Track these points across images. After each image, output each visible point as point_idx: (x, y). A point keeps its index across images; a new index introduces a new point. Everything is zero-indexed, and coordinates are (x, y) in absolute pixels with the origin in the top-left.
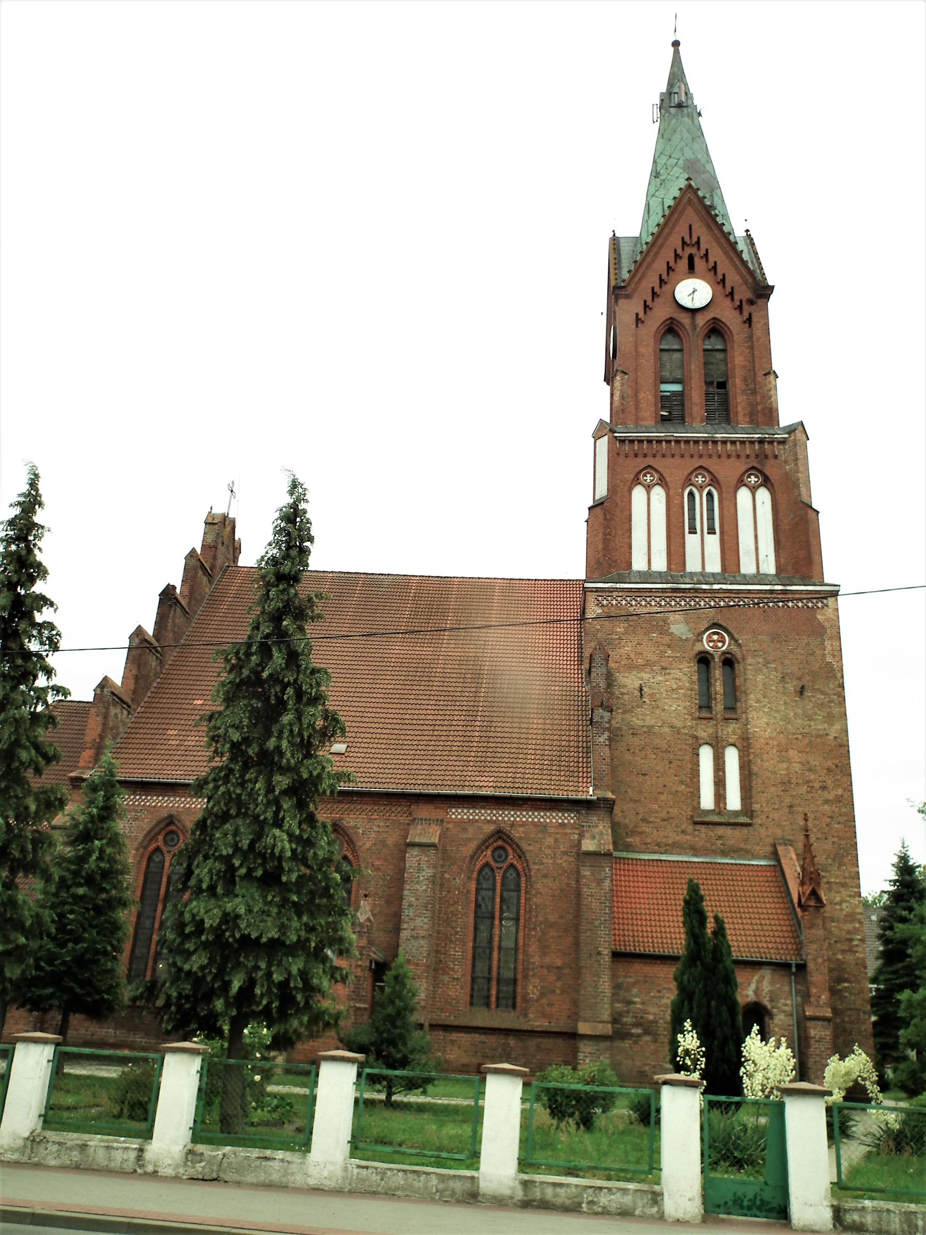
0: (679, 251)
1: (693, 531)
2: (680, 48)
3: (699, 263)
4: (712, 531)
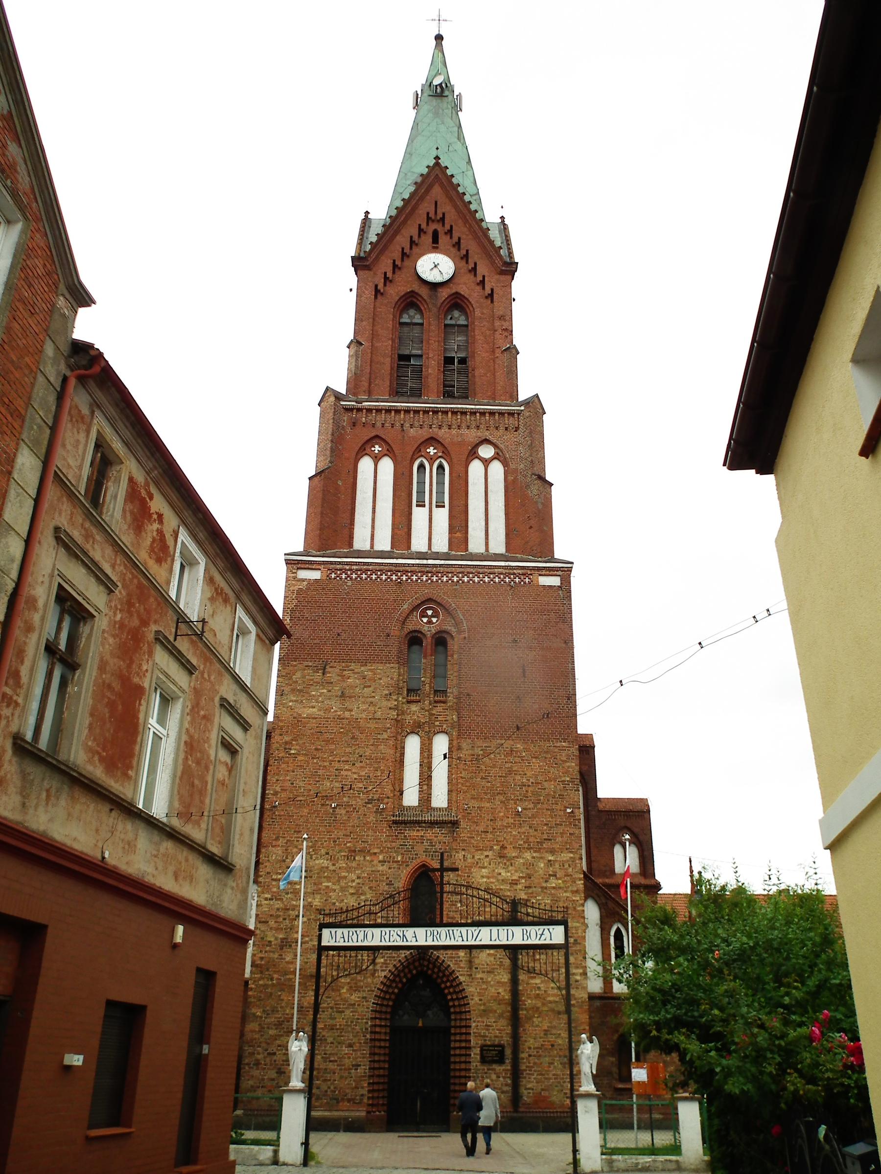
0: (424, 226)
2: (443, 43)
3: (443, 239)
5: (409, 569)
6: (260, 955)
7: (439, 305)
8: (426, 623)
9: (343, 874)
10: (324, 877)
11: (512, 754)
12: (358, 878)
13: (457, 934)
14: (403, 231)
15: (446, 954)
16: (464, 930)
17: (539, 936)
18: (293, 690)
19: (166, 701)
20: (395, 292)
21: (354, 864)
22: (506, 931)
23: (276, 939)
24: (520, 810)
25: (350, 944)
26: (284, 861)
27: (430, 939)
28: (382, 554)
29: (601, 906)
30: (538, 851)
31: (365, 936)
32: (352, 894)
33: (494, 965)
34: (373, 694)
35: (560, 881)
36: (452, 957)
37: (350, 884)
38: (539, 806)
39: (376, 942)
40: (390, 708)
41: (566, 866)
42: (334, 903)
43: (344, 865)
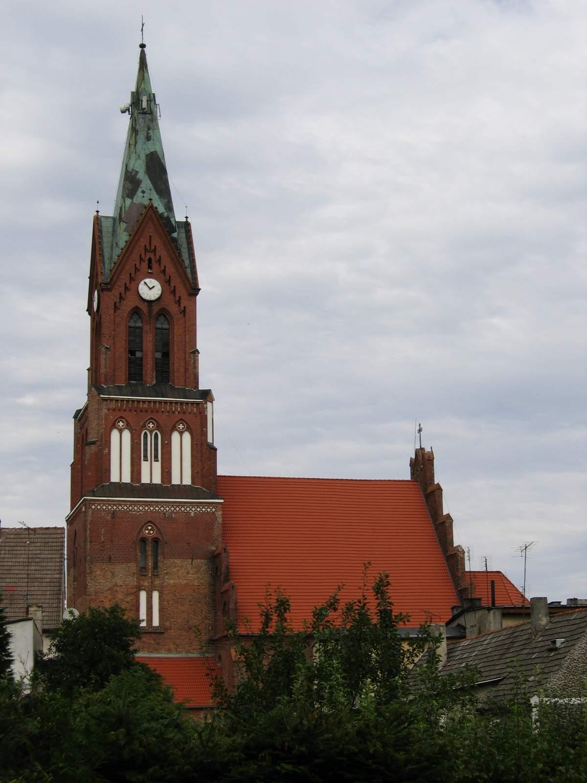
1: (146, 457)
3: (155, 266)
4: (156, 460)
28: (181, 491)
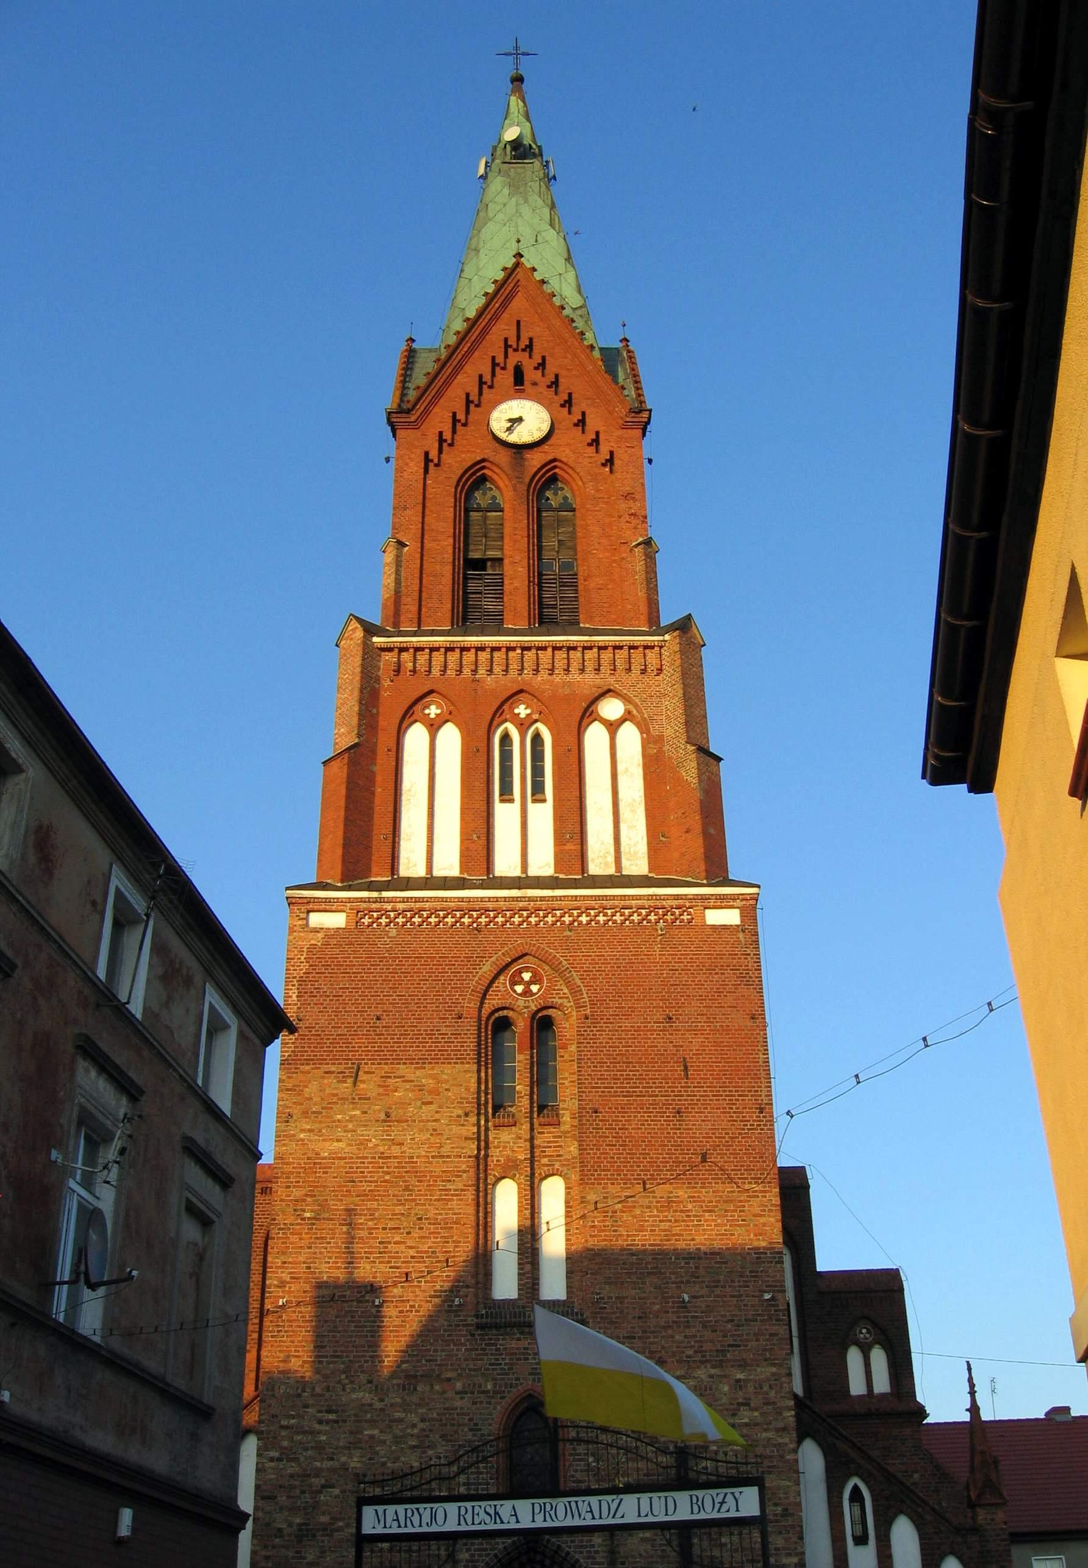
0: (500, 359)
5: (490, 905)
6: (263, 1553)
7: (527, 480)
8: (520, 995)
9: (397, 1415)
10: (366, 1421)
11: (669, 1207)
12: (423, 1420)
13: (584, 1508)
14: (467, 368)
15: (572, 1541)
16: (594, 1500)
17: (717, 1506)
18: (305, 1113)
19: (96, 1141)
20: (456, 461)
21: (415, 1398)
22: (663, 1499)
23: (290, 1525)
24: (686, 1297)
25: (410, 1530)
26: (299, 1396)
27: (539, 1518)
28: (446, 883)
29: (828, 1453)
30: (720, 1364)
31: (433, 1517)
32: (414, 1447)
33: (652, 1557)
34: (437, 1116)
35: (756, 1414)
36: (582, 1546)
37: (409, 1431)
38: (718, 1291)
39: (451, 1526)
40: (466, 1139)
41: (766, 1388)
42: (384, 1464)
43: (398, 1400)
